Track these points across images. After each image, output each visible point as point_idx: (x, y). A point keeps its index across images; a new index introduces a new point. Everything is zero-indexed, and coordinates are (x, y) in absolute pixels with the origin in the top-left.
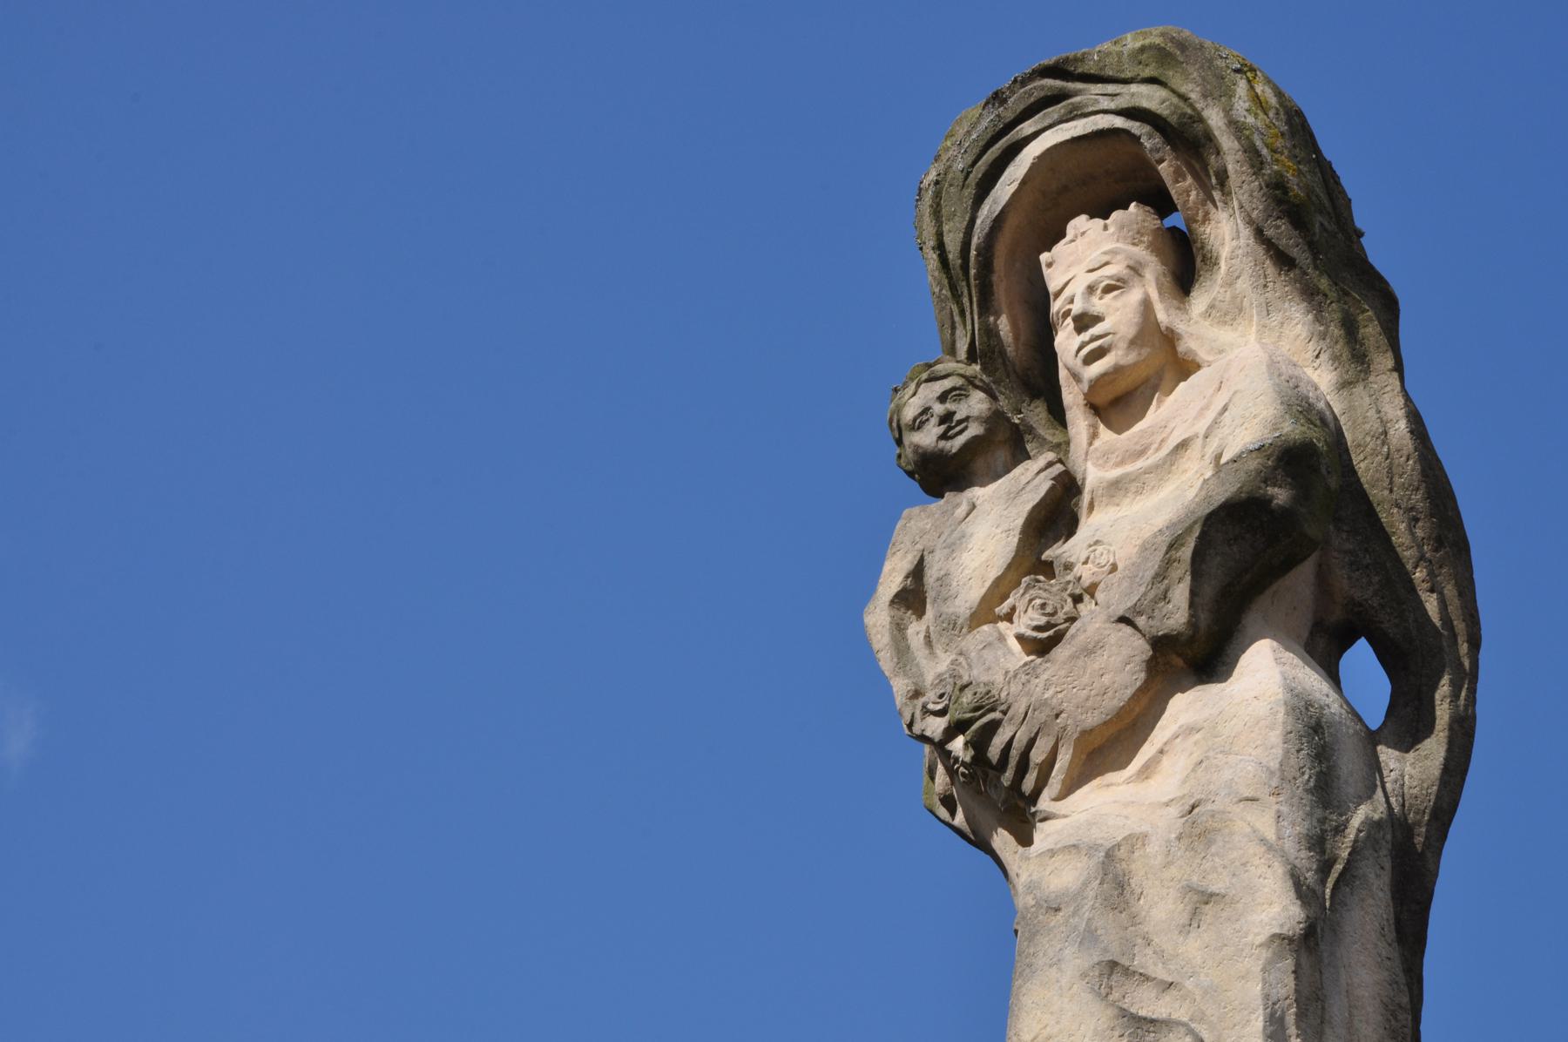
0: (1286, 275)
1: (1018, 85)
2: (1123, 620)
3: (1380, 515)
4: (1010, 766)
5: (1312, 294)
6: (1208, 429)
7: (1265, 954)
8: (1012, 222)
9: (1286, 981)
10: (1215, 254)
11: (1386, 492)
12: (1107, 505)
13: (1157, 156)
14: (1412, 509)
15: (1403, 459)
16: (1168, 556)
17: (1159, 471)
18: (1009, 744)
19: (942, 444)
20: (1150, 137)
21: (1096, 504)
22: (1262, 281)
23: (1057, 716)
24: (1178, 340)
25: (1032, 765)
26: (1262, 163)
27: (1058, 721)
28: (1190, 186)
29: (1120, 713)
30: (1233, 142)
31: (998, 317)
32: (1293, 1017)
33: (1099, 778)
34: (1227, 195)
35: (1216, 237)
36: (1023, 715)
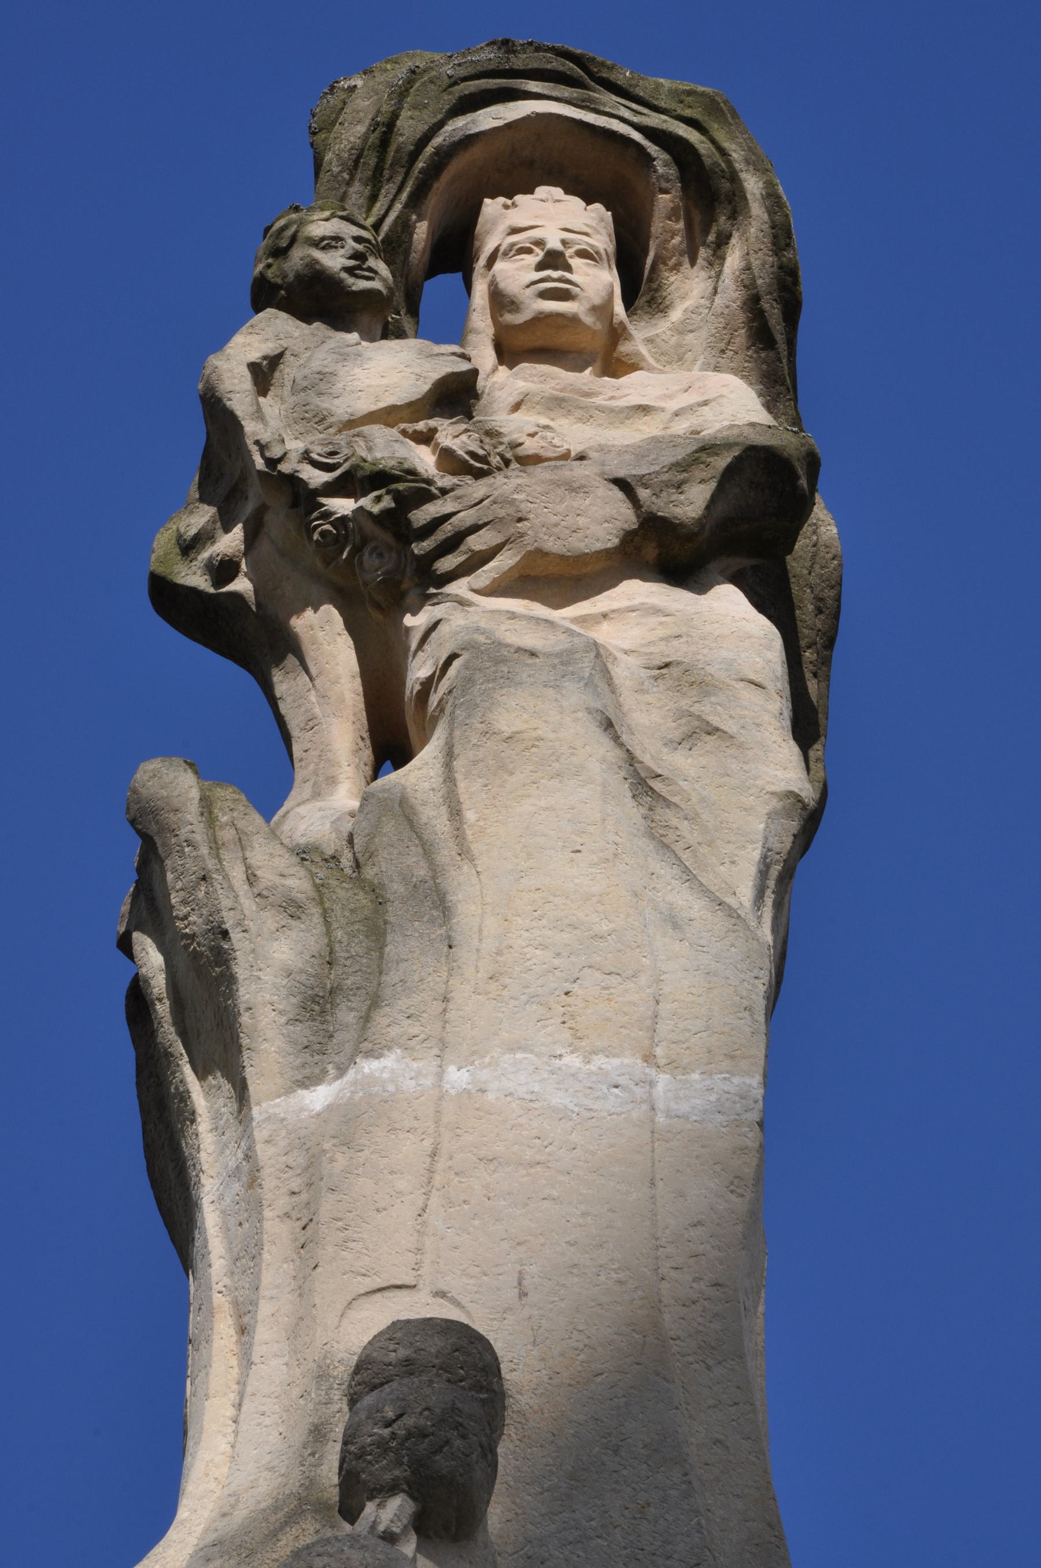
0: (756, 352)
1: (532, 48)
2: (622, 484)
3: (792, 586)
4: (433, 538)
5: (776, 382)
6: (682, 409)
7: (775, 803)
8: (476, 152)
9: (784, 838)
10: (668, 303)
11: (805, 572)
12: (539, 413)
13: (664, 185)
14: (821, 600)
15: (830, 556)
16: (696, 455)
17: (611, 415)
18: (447, 517)
19: (344, 275)
20: (666, 164)
21: (523, 407)
22: (722, 345)
23: (520, 520)
24: (626, 339)
25: (463, 548)
26: (788, 245)
27: (519, 525)
28: (679, 230)
29: (581, 559)
30: (763, 213)
31: (420, 219)
32: (776, 873)
33: (527, 601)
34: (718, 257)
35: (678, 289)
36: (477, 501)
